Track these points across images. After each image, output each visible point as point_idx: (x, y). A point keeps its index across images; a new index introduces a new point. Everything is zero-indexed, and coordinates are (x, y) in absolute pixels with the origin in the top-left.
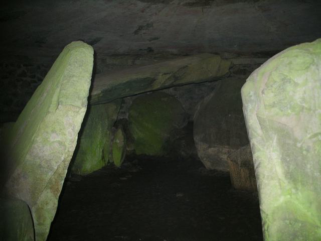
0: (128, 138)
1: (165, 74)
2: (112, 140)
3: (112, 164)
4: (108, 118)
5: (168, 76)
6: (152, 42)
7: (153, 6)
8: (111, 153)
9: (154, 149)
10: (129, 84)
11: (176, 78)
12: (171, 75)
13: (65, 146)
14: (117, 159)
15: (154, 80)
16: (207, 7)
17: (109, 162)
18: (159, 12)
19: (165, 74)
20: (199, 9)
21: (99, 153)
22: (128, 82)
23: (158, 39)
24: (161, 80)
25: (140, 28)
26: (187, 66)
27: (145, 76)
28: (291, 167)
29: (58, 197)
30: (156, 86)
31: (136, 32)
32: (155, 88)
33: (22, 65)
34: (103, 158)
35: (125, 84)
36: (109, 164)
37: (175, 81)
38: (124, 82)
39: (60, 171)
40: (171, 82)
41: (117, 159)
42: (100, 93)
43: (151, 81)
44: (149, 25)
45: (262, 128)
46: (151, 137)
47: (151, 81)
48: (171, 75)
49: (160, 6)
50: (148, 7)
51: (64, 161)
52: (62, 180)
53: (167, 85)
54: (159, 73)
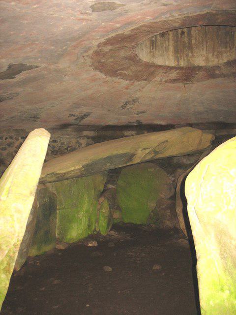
0: (115, 206)
1: (144, 149)
2: (99, 210)
3: (99, 233)
4: (95, 189)
5: (147, 151)
6: (140, 115)
7: (137, 83)
8: (97, 221)
9: (138, 218)
10: (110, 159)
11: (156, 153)
12: (150, 149)
13: (229, 272)
14: (102, 227)
15: (133, 155)
16: (189, 82)
17: (95, 230)
18: (143, 88)
19: (144, 149)
20: (180, 84)
21: (84, 222)
22: (108, 157)
23: (145, 112)
24: (141, 155)
25: (127, 103)
26: (167, 141)
27: (125, 151)
28: (229, 263)
29: (10, 278)
30: (136, 160)
31: (123, 107)
32: (135, 162)
33: (20, 138)
34: (89, 226)
35: (105, 159)
36: (95, 233)
37: (156, 155)
38: (105, 156)
39: (11, 254)
40: (151, 156)
41: (102, 227)
42: (82, 168)
43: (132, 156)
44: (135, 101)
45: (200, 222)
46: (138, 207)
47: (132, 156)
48: (150, 149)
49: (143, 83)
50: (132, 85)
51: (15, 245)
52: (12, 262)
53: (147, 159)
54: (139, 148)
